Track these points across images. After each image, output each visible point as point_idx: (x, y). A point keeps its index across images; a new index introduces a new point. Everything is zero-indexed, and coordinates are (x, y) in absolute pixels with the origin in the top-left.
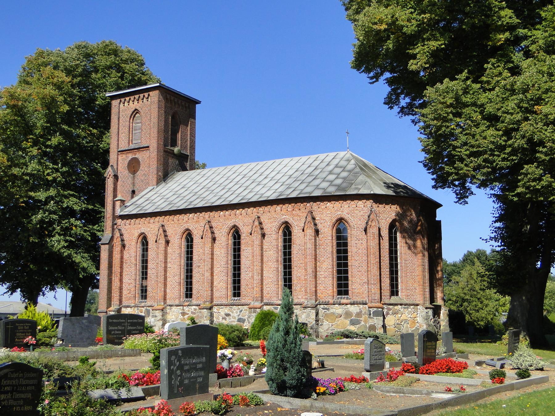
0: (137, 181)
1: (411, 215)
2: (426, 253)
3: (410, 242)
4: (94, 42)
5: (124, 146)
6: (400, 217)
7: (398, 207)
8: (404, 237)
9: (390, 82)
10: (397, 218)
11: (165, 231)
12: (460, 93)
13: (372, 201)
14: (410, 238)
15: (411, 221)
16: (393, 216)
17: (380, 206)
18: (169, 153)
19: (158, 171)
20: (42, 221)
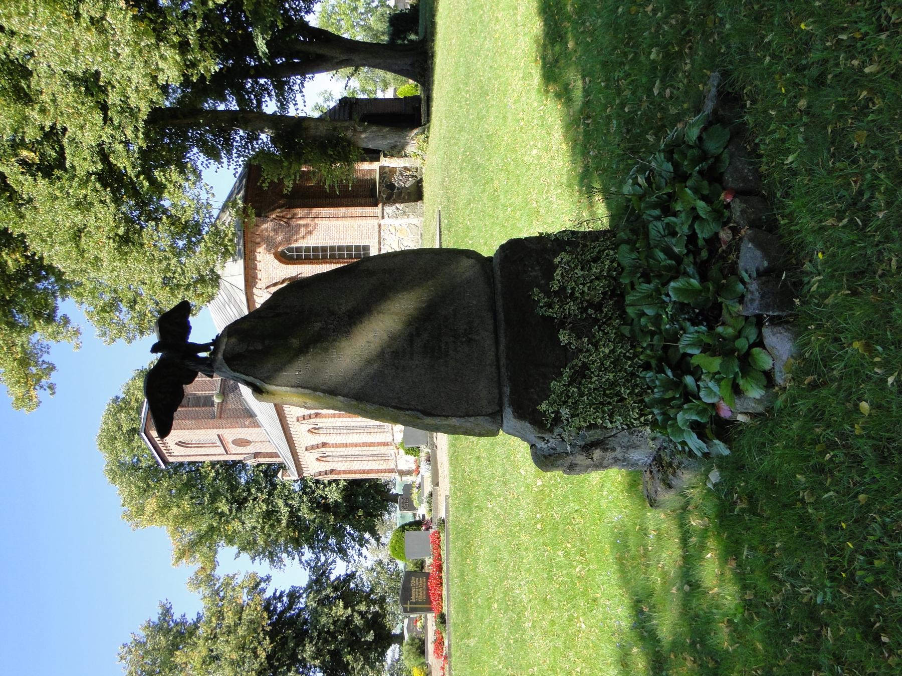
0: (258, 439)
1: (267, 230)
2: (315, 211)
3: (302, 231)
4: (102, 460)
5: (221, 450)
6: (271, 245)
7: (258, 250)
8: (296, 240)
9: (43, 177)
10: (273, 251)
11: (312, 447)
12: (140, 473)
13: (254, 289)
14: (297, 233)
15: (275, 231)
16: (270, 258)
17: (259, 277)
18: (221, 409)
19: (245, 426)
20: (312, 510)
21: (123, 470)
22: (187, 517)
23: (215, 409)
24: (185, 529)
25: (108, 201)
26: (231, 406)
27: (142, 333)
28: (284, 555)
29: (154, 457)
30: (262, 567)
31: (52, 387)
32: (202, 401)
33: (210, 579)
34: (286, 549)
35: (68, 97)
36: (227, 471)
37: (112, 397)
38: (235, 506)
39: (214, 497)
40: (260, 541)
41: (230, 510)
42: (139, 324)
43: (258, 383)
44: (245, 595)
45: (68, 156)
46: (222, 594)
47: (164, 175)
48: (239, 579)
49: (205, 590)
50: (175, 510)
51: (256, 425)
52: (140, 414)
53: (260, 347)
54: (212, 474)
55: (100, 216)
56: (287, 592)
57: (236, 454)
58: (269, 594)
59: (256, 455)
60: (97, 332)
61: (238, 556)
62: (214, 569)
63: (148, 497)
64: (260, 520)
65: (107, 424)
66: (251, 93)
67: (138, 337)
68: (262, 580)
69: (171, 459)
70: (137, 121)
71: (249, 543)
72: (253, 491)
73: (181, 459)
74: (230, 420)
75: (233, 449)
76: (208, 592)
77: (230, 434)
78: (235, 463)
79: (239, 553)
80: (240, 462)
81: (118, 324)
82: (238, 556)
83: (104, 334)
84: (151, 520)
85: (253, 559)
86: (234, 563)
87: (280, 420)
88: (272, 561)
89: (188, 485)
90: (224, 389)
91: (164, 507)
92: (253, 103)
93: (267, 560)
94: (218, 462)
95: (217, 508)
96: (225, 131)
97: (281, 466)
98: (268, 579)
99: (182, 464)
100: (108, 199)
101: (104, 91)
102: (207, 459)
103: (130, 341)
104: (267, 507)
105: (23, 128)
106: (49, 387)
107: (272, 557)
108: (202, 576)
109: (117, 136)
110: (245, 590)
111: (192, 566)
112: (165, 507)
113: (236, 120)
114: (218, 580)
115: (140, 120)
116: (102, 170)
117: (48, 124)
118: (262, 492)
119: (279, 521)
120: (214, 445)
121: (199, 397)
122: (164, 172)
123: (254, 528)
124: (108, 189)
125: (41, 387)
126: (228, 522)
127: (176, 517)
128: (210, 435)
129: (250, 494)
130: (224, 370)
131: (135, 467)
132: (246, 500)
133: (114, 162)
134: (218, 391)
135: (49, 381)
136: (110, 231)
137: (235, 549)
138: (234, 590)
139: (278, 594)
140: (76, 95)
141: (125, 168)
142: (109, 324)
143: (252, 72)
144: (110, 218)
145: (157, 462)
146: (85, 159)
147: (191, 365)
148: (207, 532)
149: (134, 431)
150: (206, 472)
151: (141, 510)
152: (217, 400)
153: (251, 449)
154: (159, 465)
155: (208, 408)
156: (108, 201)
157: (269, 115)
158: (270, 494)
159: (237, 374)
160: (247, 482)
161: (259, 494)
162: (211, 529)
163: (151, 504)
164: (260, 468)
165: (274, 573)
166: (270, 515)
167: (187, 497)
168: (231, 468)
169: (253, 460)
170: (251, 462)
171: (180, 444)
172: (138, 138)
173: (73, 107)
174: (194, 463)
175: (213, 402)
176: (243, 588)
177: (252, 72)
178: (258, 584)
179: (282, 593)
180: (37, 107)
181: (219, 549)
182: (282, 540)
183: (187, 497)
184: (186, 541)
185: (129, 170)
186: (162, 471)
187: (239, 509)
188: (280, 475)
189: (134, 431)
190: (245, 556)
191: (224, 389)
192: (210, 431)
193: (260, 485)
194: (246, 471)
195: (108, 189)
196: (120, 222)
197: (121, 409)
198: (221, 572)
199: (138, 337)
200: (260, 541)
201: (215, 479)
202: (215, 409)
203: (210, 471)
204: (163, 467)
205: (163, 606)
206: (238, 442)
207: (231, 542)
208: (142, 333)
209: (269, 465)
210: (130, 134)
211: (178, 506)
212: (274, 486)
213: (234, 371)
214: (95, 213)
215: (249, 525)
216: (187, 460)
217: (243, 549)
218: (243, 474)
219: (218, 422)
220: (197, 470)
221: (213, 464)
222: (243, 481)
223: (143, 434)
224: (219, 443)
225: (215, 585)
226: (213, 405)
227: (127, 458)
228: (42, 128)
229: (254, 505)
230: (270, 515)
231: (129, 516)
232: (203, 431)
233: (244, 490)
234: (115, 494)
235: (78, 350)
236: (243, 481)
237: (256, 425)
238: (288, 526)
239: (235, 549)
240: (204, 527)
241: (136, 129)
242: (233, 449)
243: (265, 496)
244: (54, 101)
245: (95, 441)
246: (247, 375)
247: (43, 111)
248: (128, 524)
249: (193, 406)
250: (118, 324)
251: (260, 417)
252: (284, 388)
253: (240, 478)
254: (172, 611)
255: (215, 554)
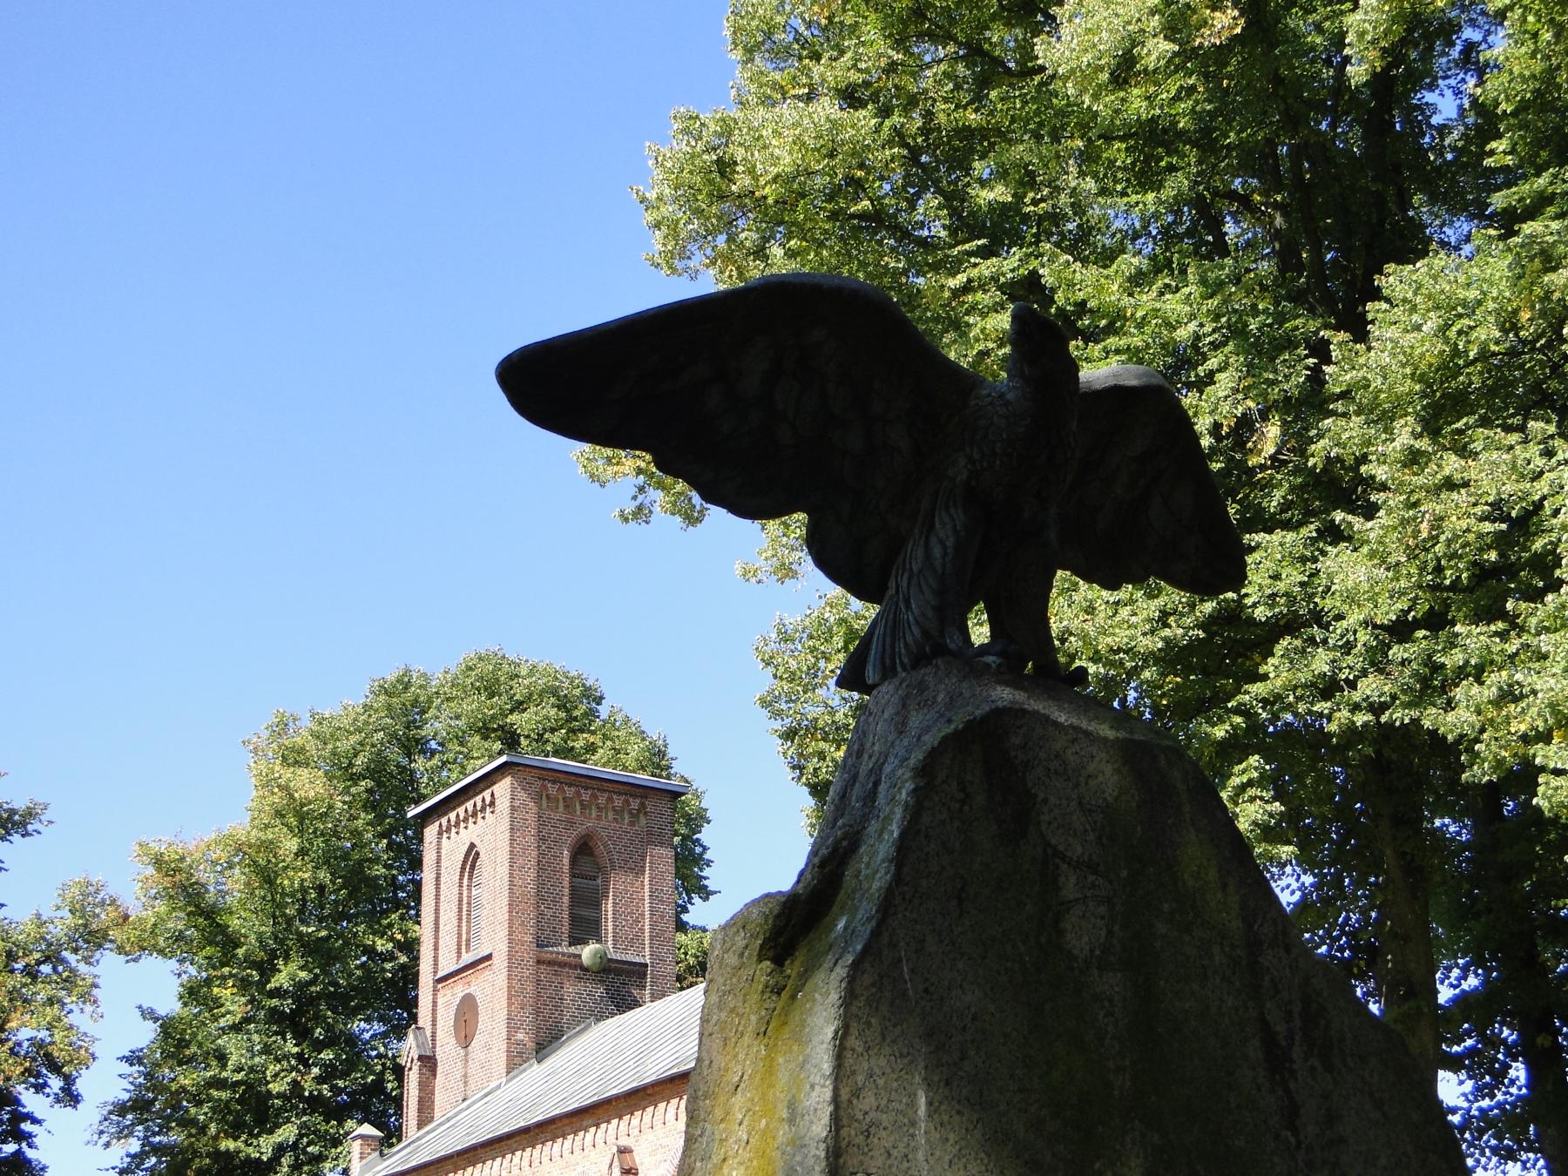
4: (437, 659)
5: (448, 965)
12: (395, 754)
18: (563, 965)
19: (512, 1028)
21: (405, 708)
22: (268, 877)
23: (564, 948)
24: (237, 871)
25: (1167, 632)
26: (572, 990)
27: (789, 735)
28: (134, 1146)
29: (437, 792)
30: (106, 1083)
31: (641, 513)
32: (585, 912)
33: (92, 938)
34: (157, 1150)
35: (1462, 519)
36: (390, 983)
37: (605, 688)
38: (288, 1005)
39: (317, 952)
40: (188, 1079)
41: (278, 993)
42: (813, 729)
43: (848, 924)
44: (33, 1033)
45: (1277, 536)
46: (46, 969)
47: (1250, 783)
48: (80, 1018)
49: (61, 926)
50: (291, 844)
51: (516, 1061)
52: (556, 753)
53: (1083, 933)
54: (382, 945)
55: (1124, 612)
56: (30, 1153)
57: (435, 1006)
58: (31, 1101)
59: (429, 1062)
60: (793, 619)
61: (148, 1014)
62: (121, 950)
63: (330, 777)
64: (240, 1076)
65: (531, 673)
66: (1482, 1037)
67: (777, 725)
68: (69, 1080)
69: (430, 832)
70: (1406, 705)
71: (182, 1044)
72: (327, 1055)
73: (429, 858)
74: (530, 988)
75: (451, 997)
76: (57, 931)
77: (492, 992)
78: (411, 1004)
79: (156, 1020)
80: (413, 1018)
81: (813, 671)
82: (148, 1014)
83: (785, 637)
84: (268, 783)
85: (133, 1059)
86: (126, 1005)
87: (525, 1131)
88: (121, 1109)
89: (356, 879)
90: (618, 972)
91: (299, 815)
92: (1451, 1043)
93: (126, 1096)
94: (415, 959)
95: (287, 958)
96: (1371, 964)
97: (391, 1135)
98: (70, 1097)
99: (416, 863)
100: (1174, 631)
101: (1489, 612)
102: (425, 931)
103: (764, 703)
104: (279, 1095)
105: (1358, 414)
106: (640, 508)
107: (136, 1108)
108: (105, 917)
109: (1350, 660)
110: (43, 1034)
111: (132, 890)
112: (301, 818)
113: (1411, 994)
114: (87, 960)
115: (1415, 713)
116: (1251, 621)
117: (1381, 473)
118: (320, 1080)
119: (235, 1130)
120: (462, 944)
121: (596, 905)
122: (1260, 782)
123: (222, 1058)
124: (1202, 635)
125: (641, 489)
126: (244, 985)
127: (269, 846)
128: (494, 935)
129: (319, 1046)
130: (915, 721)
131: (413, 745)
132: (302, 1035)
133: (1278, 650)
134: (612, 955)
135: (657, 509)
136: (1084, 637)
137: (169, 1003)
138: (51, 1002)
139: (26, 1126)
140: (1471, 537)
141: (1265, 677)
142: (813, 650)
143: (1542, 1040)
144: (1120, 637)
145: (423, 798)
146: (1276, 577)
147: (942, 537)
148: (222, 929)
149: (511, 740)
150: (390, 926)
151: (295, 758)
152: (587, 952)
153: (447, 1048)
154: (417, 802)
155: (566, 928)
156: (1167, 632)
157: (1436, 1095)
158: (315, 1103)
159: (897, 794)
160: (352, 1040)
161: (316, 1071)
162: (230, 942)
163: (310, 785)
164: (389, 1076)
165: (90, 1112)
166: (255, 1109)
167: (324, 876)
168: (396, 996)
169: (415, 1054)
170: (409, 1049)
171: (472, 857)
172: (1352, 711)
173: (1434, 539)
174: (417, 895)
175: (585, 942)
176: (50, 1027)
177: (1542, 1040)
178: (56, 1068)
179: (27, 1137)
180: (1424, 444)
181: (173, 964)
182: (176, 1137)
183: (324, 876)
184: (204, 875)
185: (1258, 689)
186: (401, 811)
187: (275, 1016)
188: (367, 1129)
189: (511, 740)
190: (145, 1035)
191: (618, 972)
192: (502, 933)
193: (344, 1075)
194: (385, 1035)
195: (1202, 635)
196: (1110, 664)
197: (564, 704)
198: (109, 965)
199: (777, 725)
200: (188, 1079)
201: (370, 951)
202: (564, 948)
203: (392, 939)
204: (412, 812)
205: (30, 814)
206: (467, 1013)
207: (193, 993)
208: (789, 735)
209: (398, 1102)
210: (1371, 687)
211: (302, 852)
212: (338, 1113)
213: (925, 771)
214: (1132, 601)
215: (235, 1048)
216: (427, 876)
217: (168, 1028)
218: (378, 1027)
219: (528, 953)
220: (397, 904)
221: (410, 946)
222: (357, 1025)
223: (504, 759)
224: (467, 958)
225: (75, 951)
226: (576, 941)
227: (435, 726)
228: (1364, 459)
229: (286, 1057)
230: (255, 1109)
231: (282, 726)
232: (503, 915)
233: (329, 1029)
234: (338, 690)
235: (739, 572)
236: (357, 1025)
237: (516, 1061)
238: (217, 1155)
239: (169, 1003)
240: (234, 923)
241: (1377, 709)
242: (451, 997)
243: (308, 1086)
244: (1450, 485)
245: (488, 645)
246: (903, 846)
247: (1413, 459)
248: (259, 727)
249: (573, 889)
250: (813, 671)
251: (535, 1073)
252: (819, 1098)
253: (368, 1020)
254: (16, 838)
255: (161, 952)
